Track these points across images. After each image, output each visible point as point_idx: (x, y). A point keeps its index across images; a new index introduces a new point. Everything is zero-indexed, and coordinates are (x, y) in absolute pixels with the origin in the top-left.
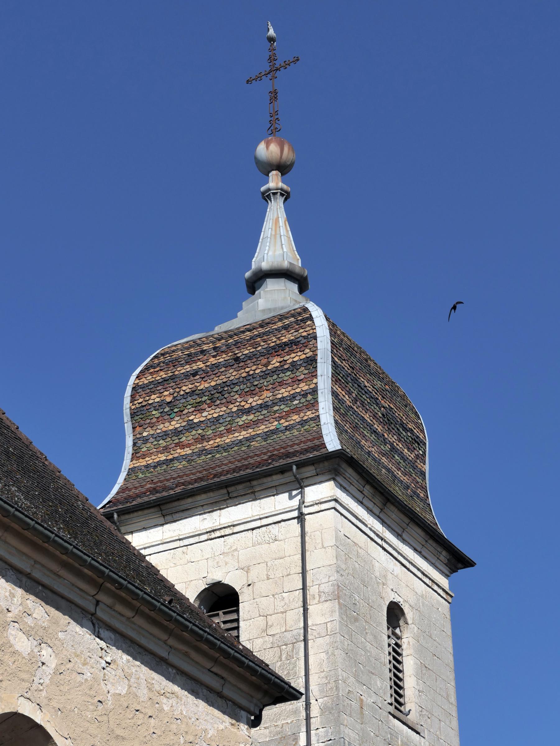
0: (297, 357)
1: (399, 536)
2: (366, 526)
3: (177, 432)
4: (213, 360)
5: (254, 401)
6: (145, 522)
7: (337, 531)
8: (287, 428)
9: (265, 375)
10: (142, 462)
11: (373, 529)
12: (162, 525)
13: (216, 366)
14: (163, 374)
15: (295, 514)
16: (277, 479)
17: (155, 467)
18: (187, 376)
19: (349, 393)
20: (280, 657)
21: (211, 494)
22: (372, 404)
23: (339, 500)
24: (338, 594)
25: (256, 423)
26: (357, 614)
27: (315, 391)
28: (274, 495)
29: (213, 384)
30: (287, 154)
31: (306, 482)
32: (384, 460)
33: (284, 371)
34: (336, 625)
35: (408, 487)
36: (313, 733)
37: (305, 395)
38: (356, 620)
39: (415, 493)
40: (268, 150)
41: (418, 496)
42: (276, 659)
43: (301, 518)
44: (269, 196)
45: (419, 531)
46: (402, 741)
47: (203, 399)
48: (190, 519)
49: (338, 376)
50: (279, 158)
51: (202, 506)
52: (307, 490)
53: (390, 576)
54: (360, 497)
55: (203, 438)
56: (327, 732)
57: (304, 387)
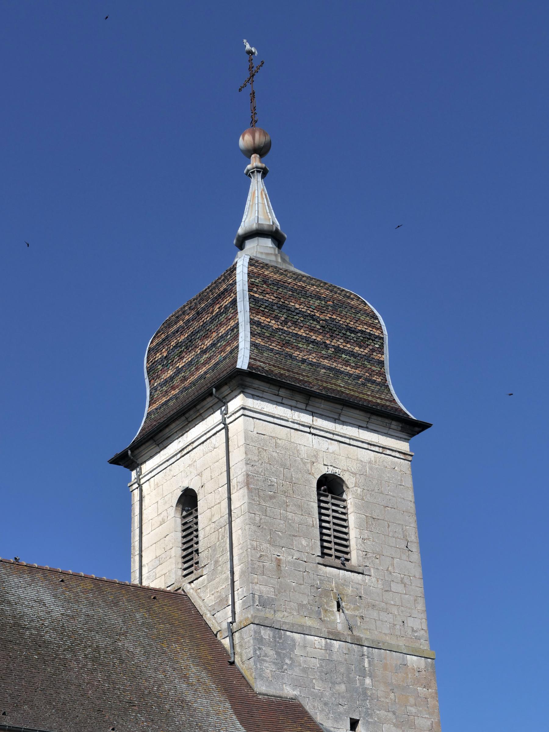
0: (227, 302)
1: (335, 420)
2: (287, 421)
3: (172, 378)
4: (187, 317)
5: (208, 342)
6: (150, 452)
7: (246, 432)
8: (225, 358)
9: (213, 320)
10: (155, 406)
11: (295, 421)
12: (159, 452)
13: (188, 321)
14: (163, 336)
15: (222, 426)
16: (210, 401)
17: (160, 407)
18: (174, 333)
19: (276, 318)
20: (218, 539)
21: (178, 422)
22: (156, 341)
23: (247, 407)
24: (248, 481)
25: (210, 358)
26: (275, 493)
27: (237, 326)
28: (213, 414)
29: (186, 336)
30: (259, 139)
31: (228, 398)
32: (326, 362)
33: (221, 314)
34: (246, 505)
35: (359, 377)
36: (235, 593)
37: (232, 330)
38: (271, 497)
39: (369, 380)
40: (245, 141)
41: (374, 382)
42: (217, 540)
43: (226, 428)
44: (250, 176)
45: (357, 412)
46: (336, 583)
47: (182, 349)
48: (172, 444)
49: (256, 305)
50: (252, 143)
51: (176, 432)
52: (230, 404)
53: (321, 454)
54: (279, 399)
55: (185, 379)
56: (243, 591)
57: (232, 323)
